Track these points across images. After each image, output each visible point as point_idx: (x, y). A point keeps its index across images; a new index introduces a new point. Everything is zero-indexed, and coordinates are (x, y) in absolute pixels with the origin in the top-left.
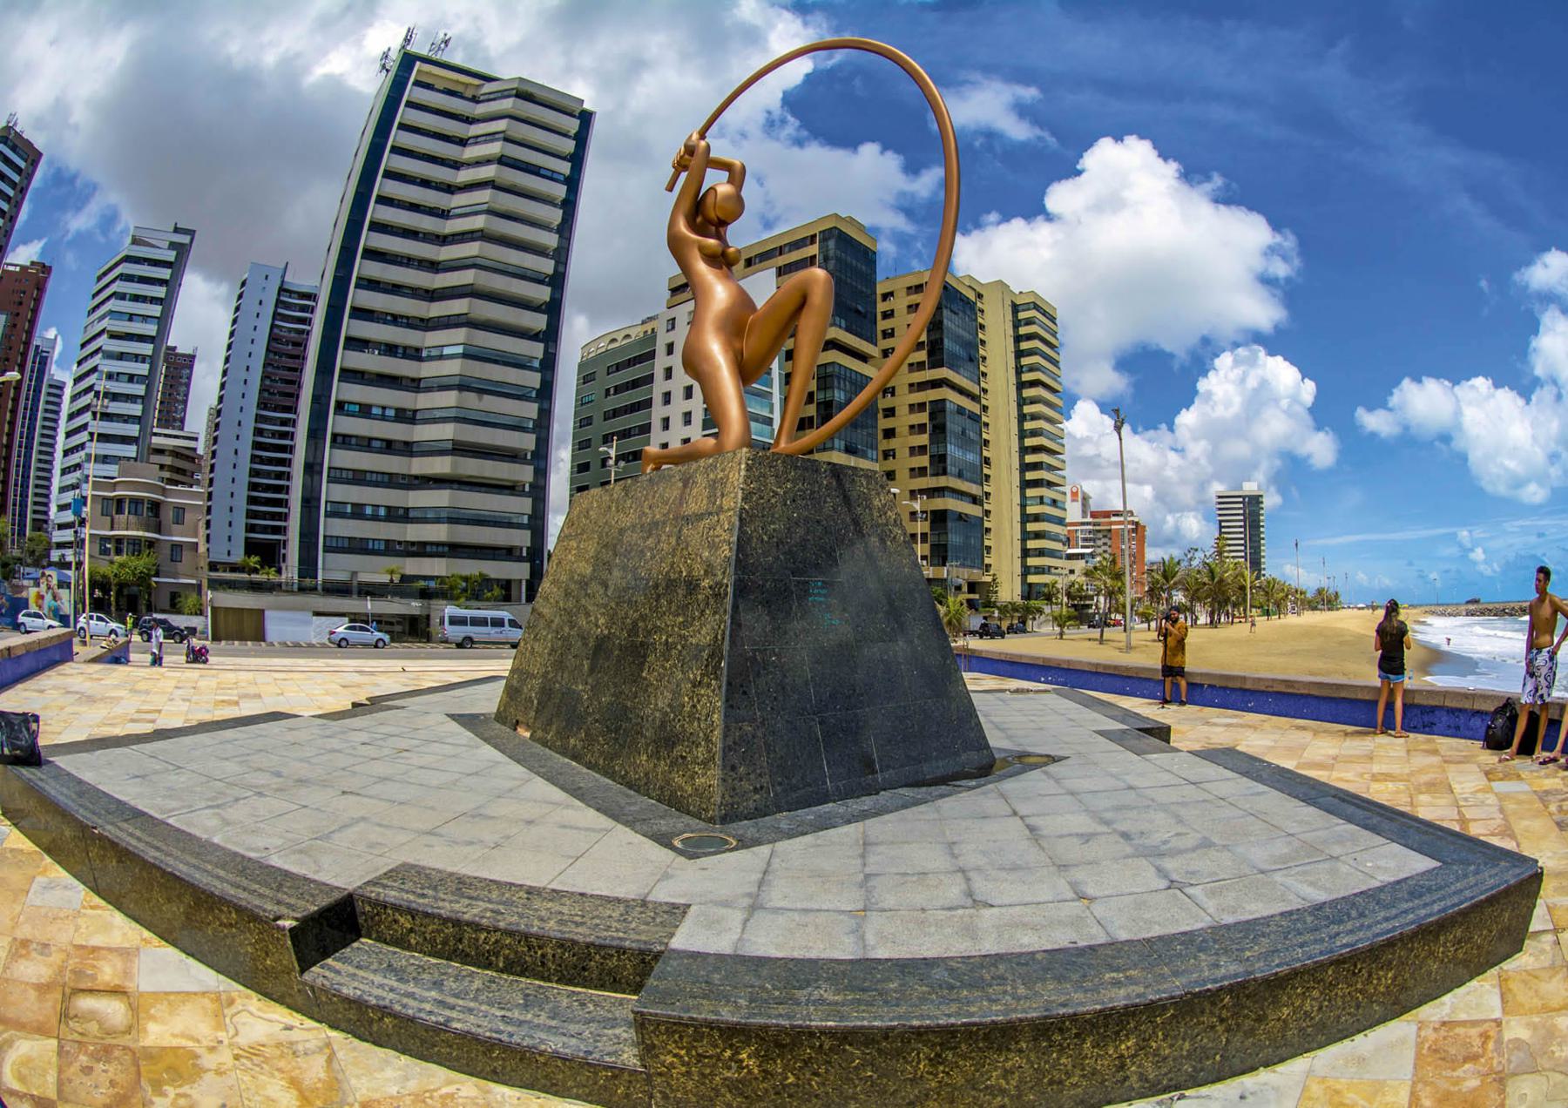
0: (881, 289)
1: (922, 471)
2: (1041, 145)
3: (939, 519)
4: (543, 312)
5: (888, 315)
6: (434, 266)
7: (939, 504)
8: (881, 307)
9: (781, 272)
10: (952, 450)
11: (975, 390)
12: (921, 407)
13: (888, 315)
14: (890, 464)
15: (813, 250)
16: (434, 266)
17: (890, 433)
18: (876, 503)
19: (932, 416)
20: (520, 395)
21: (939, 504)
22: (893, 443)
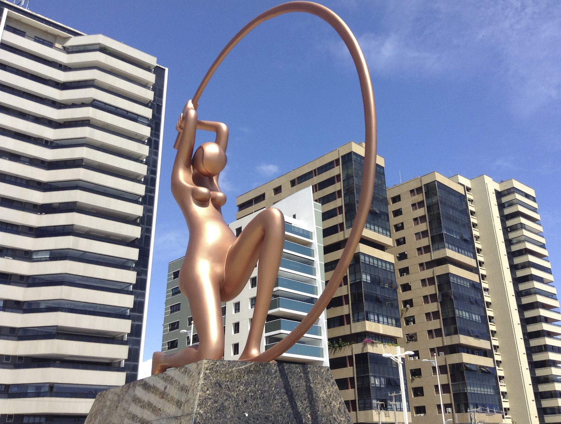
0: (390, 194)
1: (438, 333)
2: (170, 344)
3: (458, 372)
4: (138, 225)
5: (398, 213)
6: (26, 255)
7: (453, 359)
8: (392, 207)
9: (317, 188)
10: (461, 313)
11: (472, 263)
12: (431, 281)
13: (398, 213)
14: (412, 329)
15: (337, 171)
16: (26, 255)
17: (409, 303)
18: (322, 395)
19: (440, 287)
20: (118, 288)
21: (453, 359)
22: (411, 312)
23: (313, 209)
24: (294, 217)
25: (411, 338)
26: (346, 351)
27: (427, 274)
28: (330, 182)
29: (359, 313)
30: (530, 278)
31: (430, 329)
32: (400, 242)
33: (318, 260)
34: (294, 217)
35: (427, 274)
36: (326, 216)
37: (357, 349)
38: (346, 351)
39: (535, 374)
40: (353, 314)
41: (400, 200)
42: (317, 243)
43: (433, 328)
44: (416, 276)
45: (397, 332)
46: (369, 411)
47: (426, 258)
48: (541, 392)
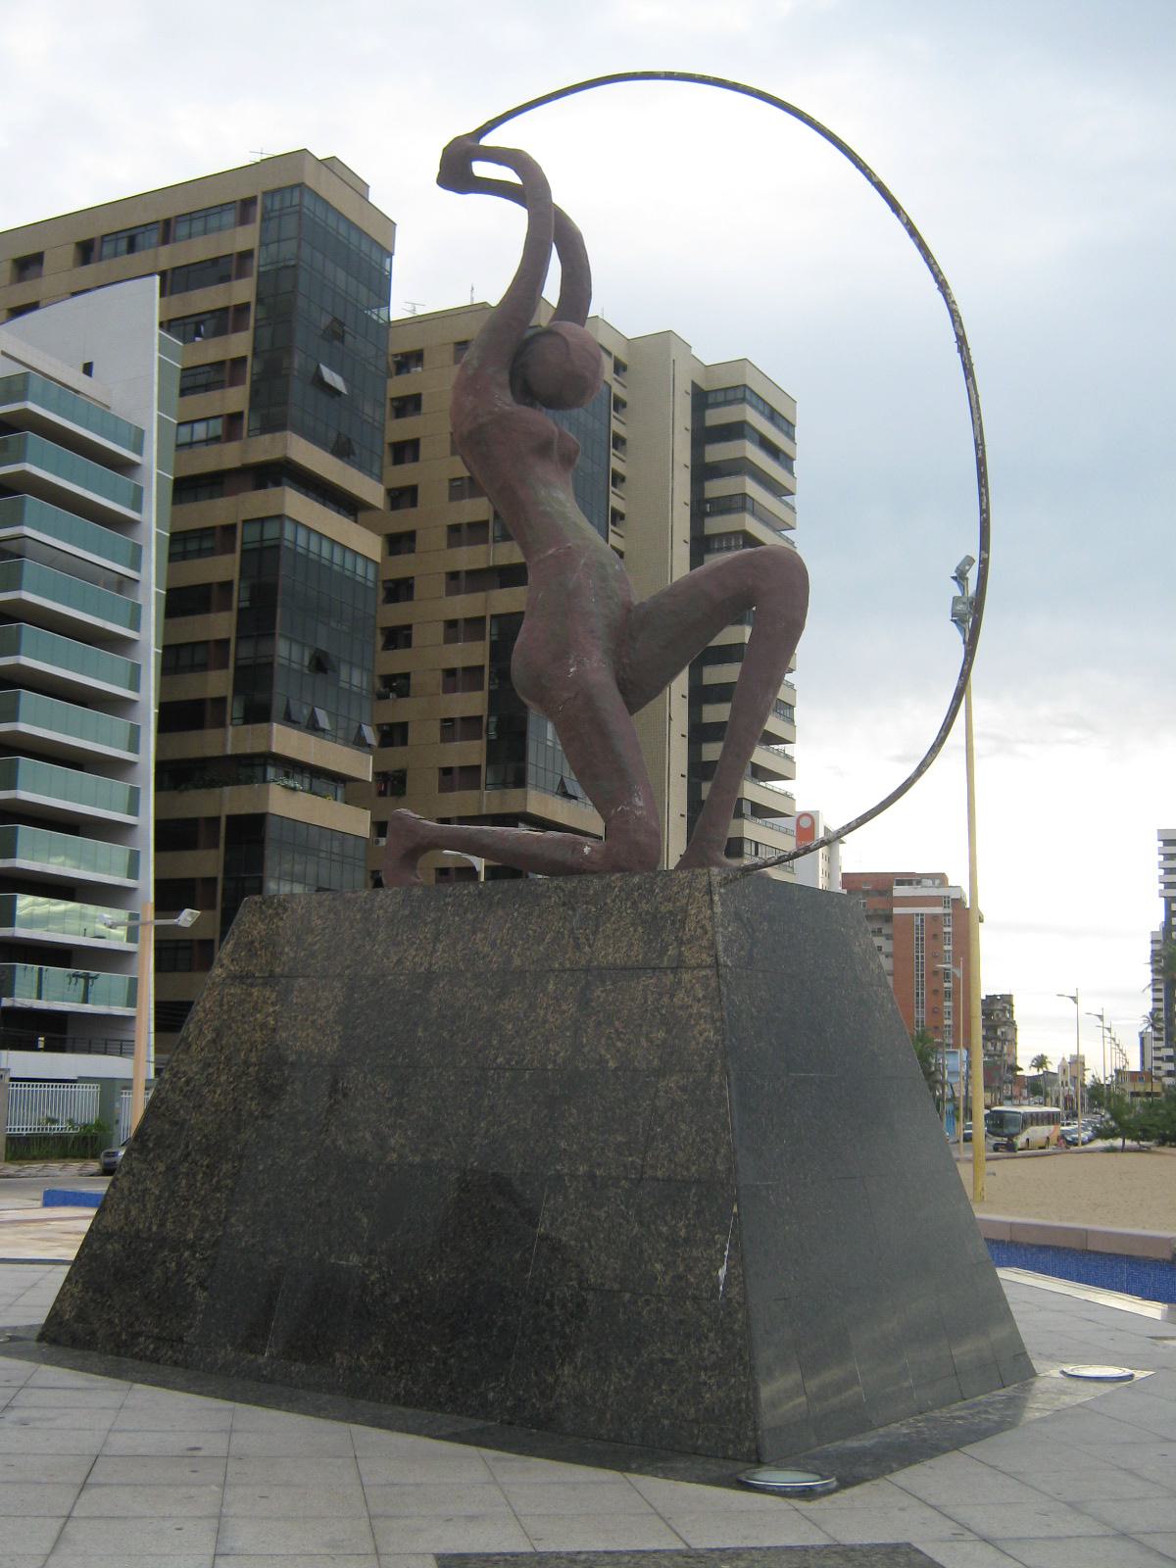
1: (469, 776)
9: (173, 282)
23: (157, 354)
24: (88, 369)
25: (391, 783)
26: (218, 511)
27: (464, 606)
28: (219, 270)
29: (270, 413)
30: (735, 431)
31: (446, 765)
32: (402, 497)
33: (152, 525)
34: (88, 369)
35: (464, 606)
36: (193, 382)
37: (233, 801)
38: (218, 511)
39: (702, 455)
40: (239, 638)
41: (409, 597)
42: (154, 471)
43: (457, 663)
44: (433, 607)
45: (370, 490)
46: (265, 725)
47: (470, 557)
48: (706, 686)
